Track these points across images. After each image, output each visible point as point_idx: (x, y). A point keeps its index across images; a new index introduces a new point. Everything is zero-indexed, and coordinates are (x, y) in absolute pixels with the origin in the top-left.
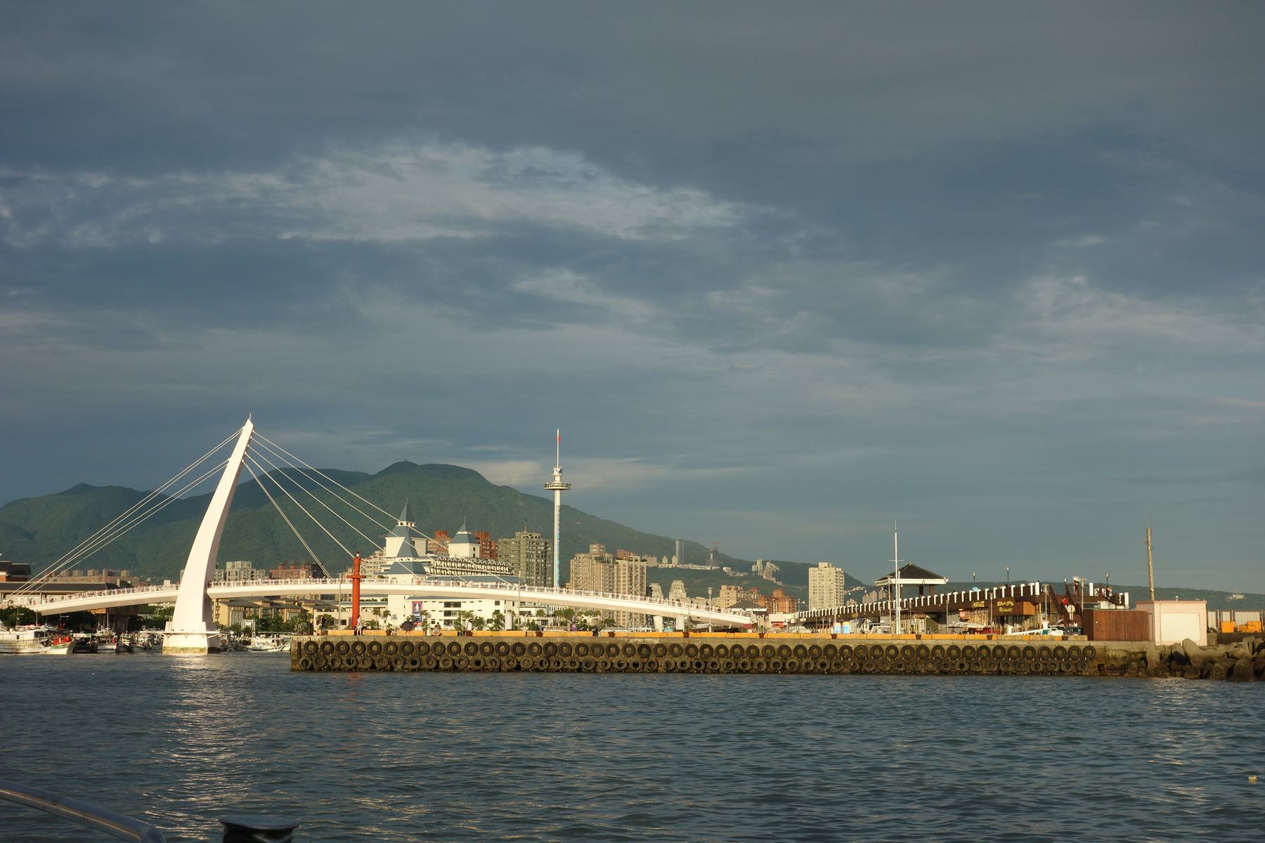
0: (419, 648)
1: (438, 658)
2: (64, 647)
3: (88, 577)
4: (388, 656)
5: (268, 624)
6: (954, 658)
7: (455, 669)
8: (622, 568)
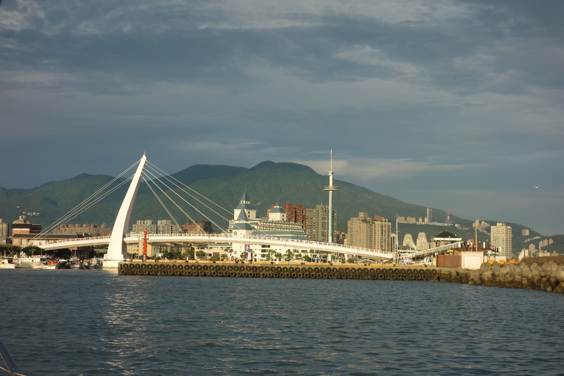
0: (161, 267)
1: (174, 271)
2: (54, 266)
3: (83, 228)
4: (155, 270)
7: (180, 275)
8: (377, 226)
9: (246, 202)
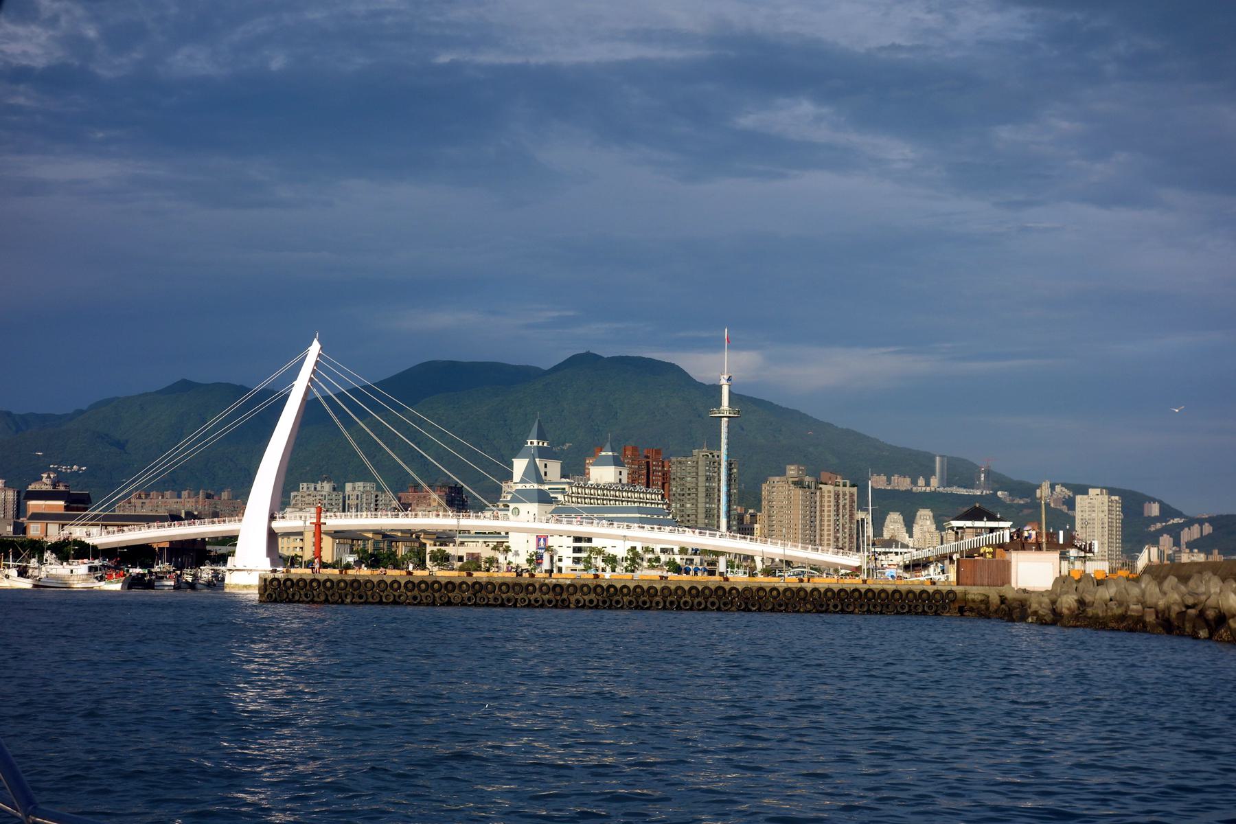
1: (381, 593)
2: (118, 582)
3: (182, 500)
5: (379, 560)
6: (870, 600)
7: (395, 603)
8: (826, 494)
9: (538, 443)
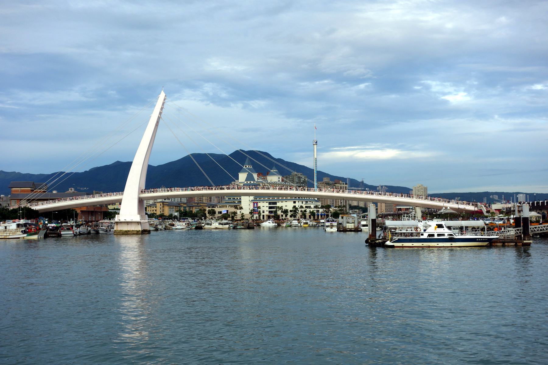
9: (248, 166)
